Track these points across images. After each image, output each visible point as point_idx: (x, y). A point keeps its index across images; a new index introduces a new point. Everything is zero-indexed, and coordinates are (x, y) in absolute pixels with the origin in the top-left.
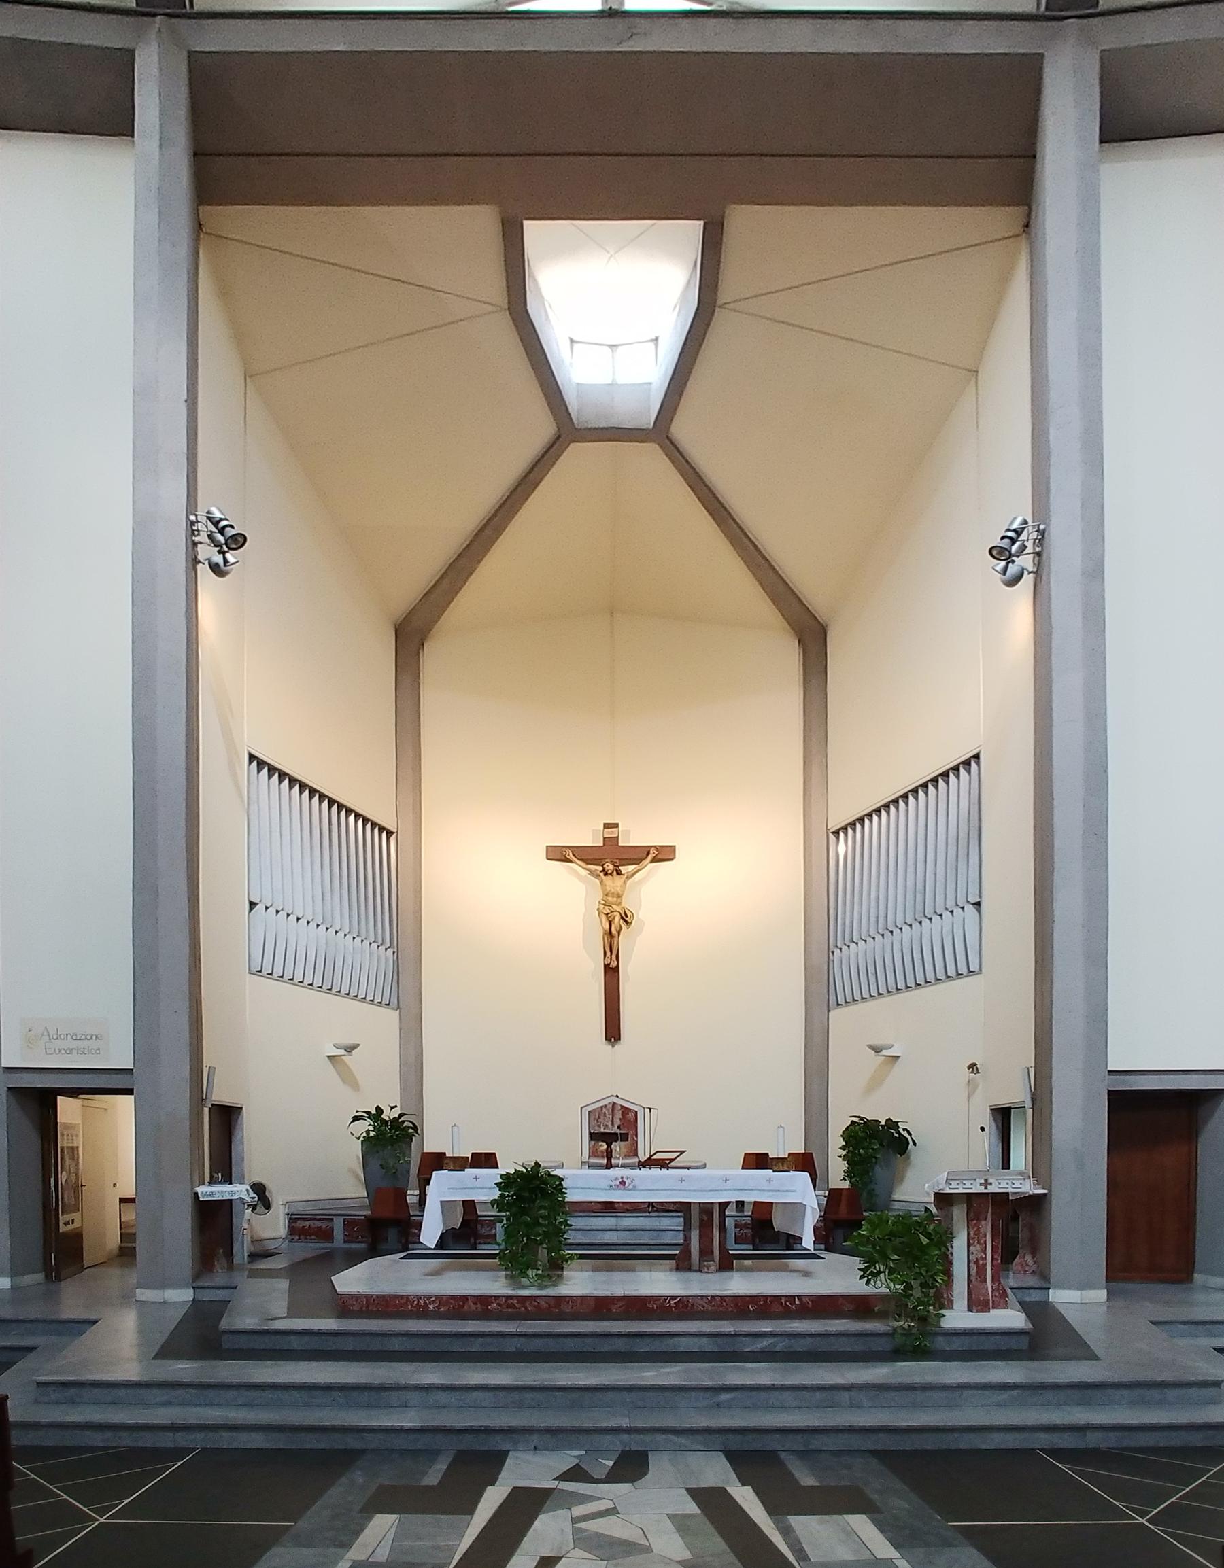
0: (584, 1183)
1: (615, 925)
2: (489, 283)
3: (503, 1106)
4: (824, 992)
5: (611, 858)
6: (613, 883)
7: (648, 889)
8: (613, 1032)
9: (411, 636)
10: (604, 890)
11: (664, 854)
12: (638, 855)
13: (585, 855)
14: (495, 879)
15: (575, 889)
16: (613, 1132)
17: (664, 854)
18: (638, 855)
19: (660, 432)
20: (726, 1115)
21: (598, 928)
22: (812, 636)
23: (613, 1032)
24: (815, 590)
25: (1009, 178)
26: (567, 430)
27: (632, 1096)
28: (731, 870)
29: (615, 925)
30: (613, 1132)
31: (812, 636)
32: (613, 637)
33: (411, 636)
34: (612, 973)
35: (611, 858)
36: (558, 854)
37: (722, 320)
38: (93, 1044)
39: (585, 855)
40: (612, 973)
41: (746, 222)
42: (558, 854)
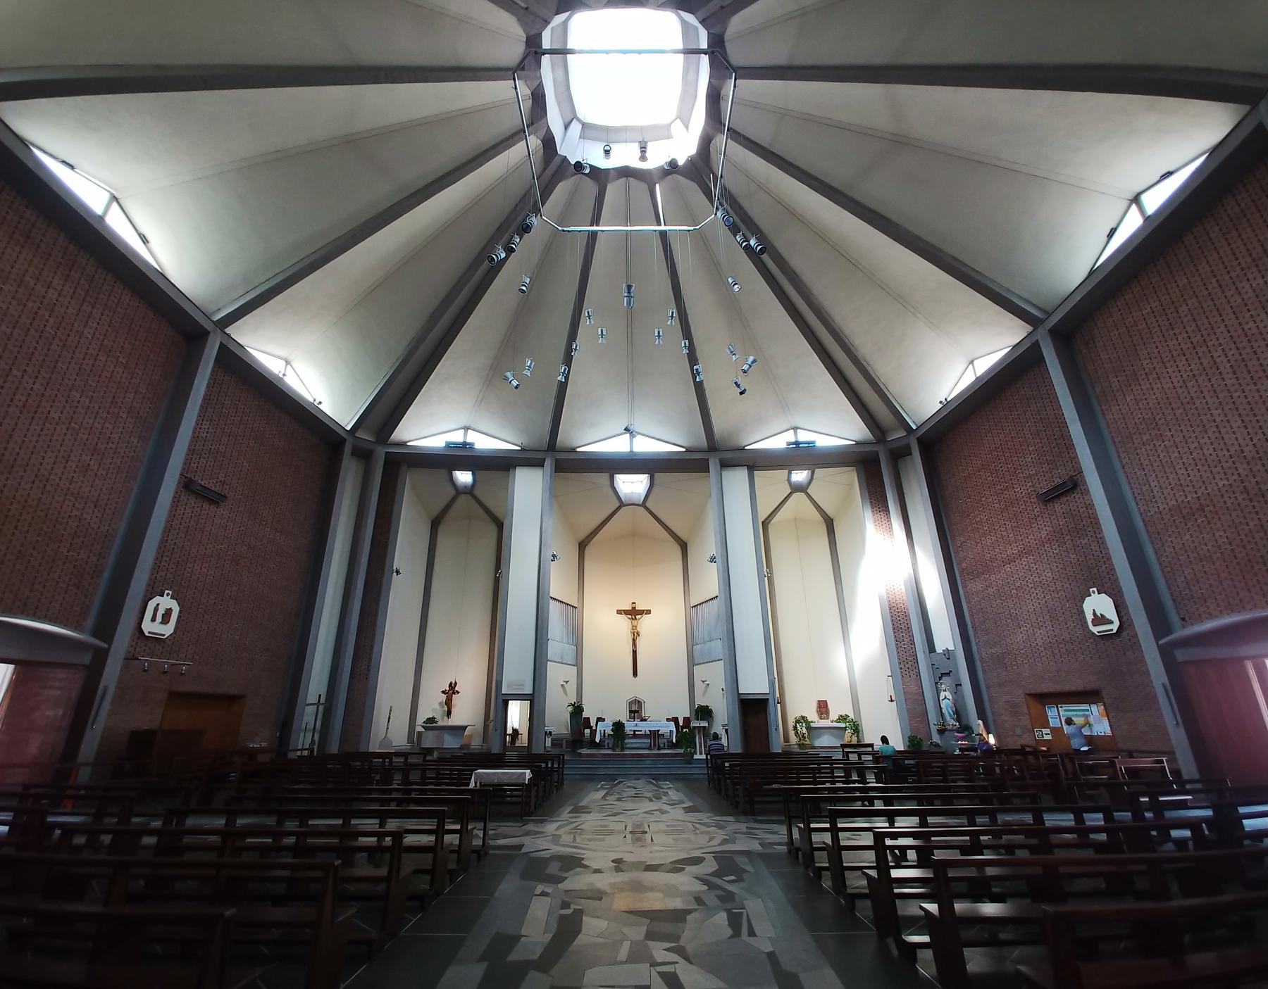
0: (818, 722)
1: (635, 635)
2: (608, 483)
3: (605, 708)
4: (692, 662)
5: (634, 613)
6: (635, 622)
7: (644, 623)
8: (635, 674)
9: (582, 546)
10: (579, 120)
11: (648, 612)
12: (642, 612)
13: (626, 612)
14: (603, 623)
15: (624, 621)
16: (636, 710)
17: (648, 612)
18: (642, 612)
19: (643, 505)
20: (665, 708)
21: (631, 637)
22: (684, 546)
23: (635, 674)
24: (684, 537)
25: (706, 469)
26: (622, 504)
27: (641, 697)
28: (666, 622)
29: (635, 635)
30: (636, 710)
31: (684, 546)
32: (633, 550)
33: (582, 546)
34: (634, 652)
35: (634, 613)
36: (619, 612)
37: (655, 489)
38: (159, 618)
39: (626, 612)
40: (634, 652)
41: (657, 475)
42: (619, 612)
